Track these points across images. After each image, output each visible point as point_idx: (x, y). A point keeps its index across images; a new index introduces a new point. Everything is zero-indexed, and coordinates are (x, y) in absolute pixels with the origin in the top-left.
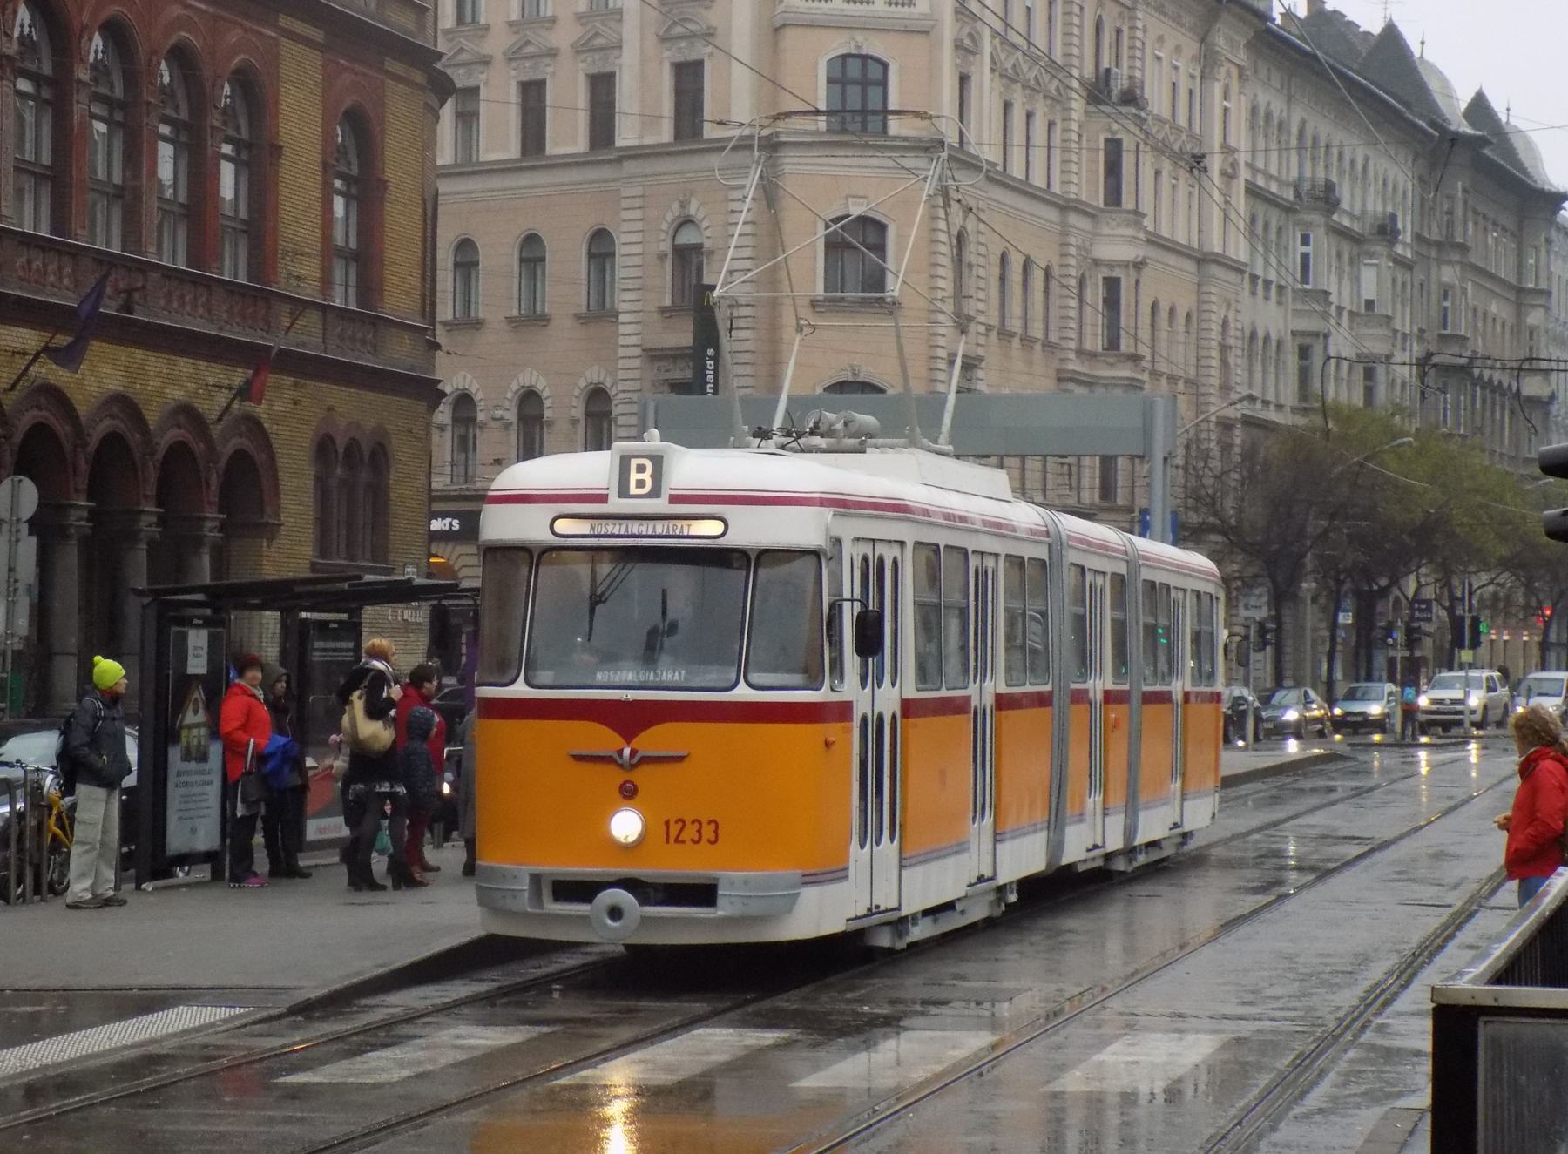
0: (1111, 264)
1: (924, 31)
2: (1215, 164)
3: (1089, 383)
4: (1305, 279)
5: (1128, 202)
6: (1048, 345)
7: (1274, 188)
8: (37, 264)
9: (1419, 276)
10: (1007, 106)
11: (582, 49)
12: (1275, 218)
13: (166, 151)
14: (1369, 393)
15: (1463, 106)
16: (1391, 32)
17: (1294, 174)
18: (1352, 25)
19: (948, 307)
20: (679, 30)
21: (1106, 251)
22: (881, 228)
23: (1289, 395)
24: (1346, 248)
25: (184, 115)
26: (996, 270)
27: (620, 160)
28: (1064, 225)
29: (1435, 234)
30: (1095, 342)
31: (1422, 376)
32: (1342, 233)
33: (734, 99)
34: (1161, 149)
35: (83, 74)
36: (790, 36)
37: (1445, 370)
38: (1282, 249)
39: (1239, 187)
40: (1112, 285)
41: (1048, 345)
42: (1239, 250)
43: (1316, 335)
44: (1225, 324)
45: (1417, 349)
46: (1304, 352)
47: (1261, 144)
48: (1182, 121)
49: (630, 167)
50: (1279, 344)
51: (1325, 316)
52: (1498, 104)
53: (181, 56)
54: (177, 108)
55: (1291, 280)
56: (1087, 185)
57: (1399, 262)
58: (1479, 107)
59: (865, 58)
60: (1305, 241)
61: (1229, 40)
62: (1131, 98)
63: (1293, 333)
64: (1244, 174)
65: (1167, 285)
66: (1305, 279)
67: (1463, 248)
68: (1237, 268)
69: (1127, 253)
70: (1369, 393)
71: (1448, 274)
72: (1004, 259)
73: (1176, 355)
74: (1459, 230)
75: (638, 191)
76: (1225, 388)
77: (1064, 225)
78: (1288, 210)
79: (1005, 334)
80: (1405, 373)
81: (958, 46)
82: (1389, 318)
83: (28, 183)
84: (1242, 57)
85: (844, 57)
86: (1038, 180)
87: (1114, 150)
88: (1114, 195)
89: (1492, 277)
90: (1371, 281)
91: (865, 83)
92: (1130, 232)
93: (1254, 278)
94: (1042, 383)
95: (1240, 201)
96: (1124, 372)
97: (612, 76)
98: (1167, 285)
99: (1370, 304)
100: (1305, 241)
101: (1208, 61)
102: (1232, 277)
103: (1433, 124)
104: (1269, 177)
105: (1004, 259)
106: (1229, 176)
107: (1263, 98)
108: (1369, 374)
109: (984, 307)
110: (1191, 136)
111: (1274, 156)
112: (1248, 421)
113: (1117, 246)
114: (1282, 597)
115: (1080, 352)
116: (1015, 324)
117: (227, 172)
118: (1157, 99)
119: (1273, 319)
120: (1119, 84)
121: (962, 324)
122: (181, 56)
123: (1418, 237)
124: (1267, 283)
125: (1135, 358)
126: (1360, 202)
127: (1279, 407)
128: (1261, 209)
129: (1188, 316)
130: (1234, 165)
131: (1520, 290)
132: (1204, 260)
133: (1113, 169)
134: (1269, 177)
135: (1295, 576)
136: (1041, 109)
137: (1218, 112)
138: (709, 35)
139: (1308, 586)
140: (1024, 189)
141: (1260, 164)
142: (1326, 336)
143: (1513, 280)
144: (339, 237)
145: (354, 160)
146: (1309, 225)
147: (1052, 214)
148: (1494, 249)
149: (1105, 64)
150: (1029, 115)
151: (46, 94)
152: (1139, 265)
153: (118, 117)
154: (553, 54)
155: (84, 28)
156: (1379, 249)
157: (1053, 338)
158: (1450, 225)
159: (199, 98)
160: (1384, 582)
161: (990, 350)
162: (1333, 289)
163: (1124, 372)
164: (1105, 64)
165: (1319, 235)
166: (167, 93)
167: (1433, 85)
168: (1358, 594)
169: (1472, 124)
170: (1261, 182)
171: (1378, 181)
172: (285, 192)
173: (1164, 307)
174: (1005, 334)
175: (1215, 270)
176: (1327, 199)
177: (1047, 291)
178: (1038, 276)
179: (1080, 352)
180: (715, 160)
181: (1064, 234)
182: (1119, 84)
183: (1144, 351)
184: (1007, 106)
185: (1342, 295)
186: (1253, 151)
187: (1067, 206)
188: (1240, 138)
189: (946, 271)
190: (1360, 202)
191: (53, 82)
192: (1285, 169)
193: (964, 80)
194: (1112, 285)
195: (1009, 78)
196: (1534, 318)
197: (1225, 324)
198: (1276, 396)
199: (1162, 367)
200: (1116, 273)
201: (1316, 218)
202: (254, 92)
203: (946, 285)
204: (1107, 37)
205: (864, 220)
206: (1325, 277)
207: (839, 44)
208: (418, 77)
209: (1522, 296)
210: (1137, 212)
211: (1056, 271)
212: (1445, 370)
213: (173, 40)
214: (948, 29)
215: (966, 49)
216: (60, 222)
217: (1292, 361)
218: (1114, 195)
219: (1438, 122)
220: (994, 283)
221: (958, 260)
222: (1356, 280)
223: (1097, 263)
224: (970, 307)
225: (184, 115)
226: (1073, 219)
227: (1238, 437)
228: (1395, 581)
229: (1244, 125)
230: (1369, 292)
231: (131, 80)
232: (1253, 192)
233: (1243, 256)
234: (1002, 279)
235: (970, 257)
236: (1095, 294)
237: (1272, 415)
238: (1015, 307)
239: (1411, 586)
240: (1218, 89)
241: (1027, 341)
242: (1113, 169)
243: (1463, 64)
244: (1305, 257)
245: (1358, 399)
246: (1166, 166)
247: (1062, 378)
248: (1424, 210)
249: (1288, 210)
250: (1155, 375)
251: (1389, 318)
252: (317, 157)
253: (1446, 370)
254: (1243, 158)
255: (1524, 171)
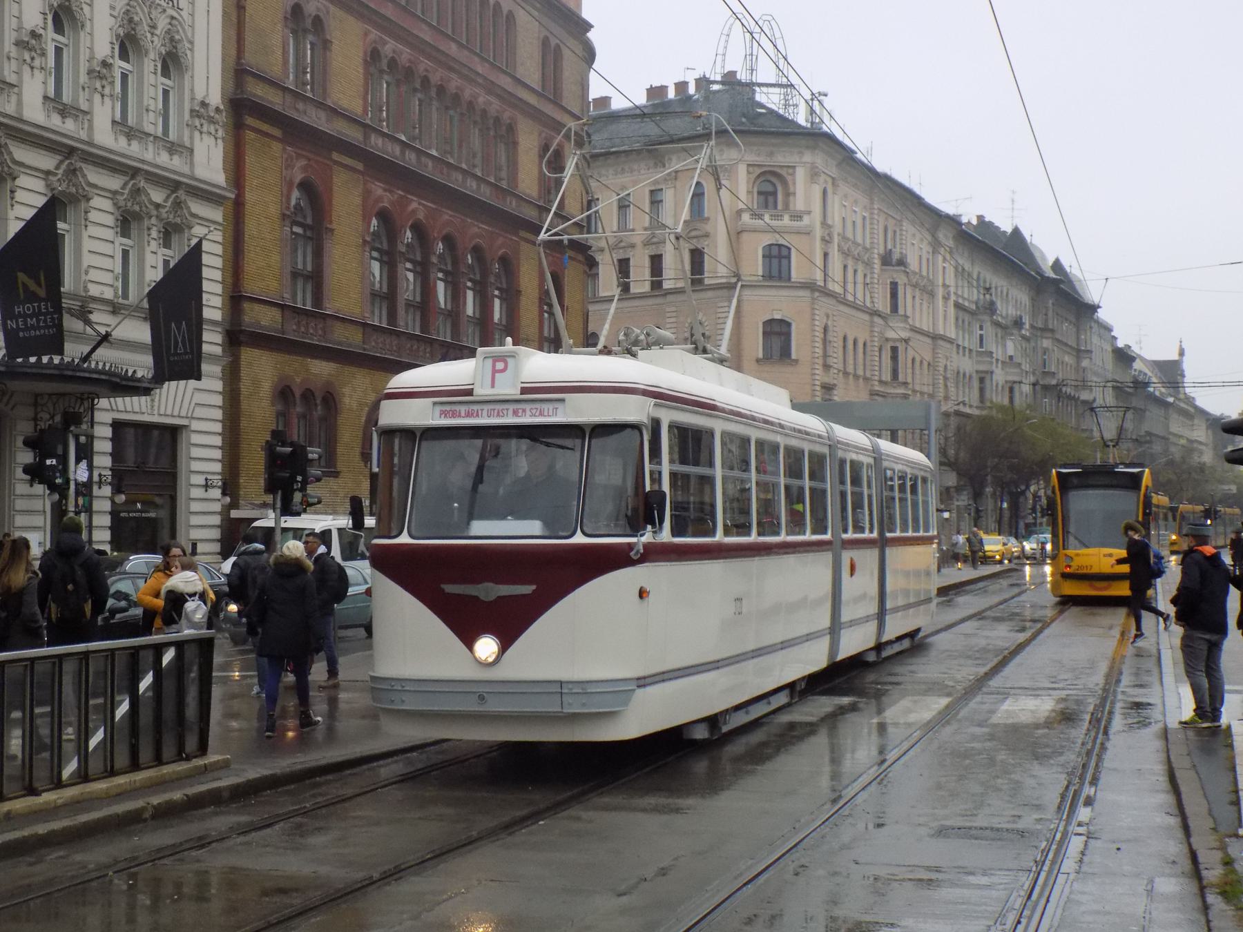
0: (894, 340)
1: (808, 233)
2: (940, 292)
3: (884, 396)
4: (981, 346)
5: (901, 311)
6: (866, 379)
7: (966, 304)
8: (388, 341)
9: (1033, 344)
10: (845, 267)
11: (647, 243)
12: (967, 317)
13: (470, 295)
14: (1011, 399)
15: (1050, 264)
16: (1016, 232)
17: (975, 297)
18: (997, 228)
19: (820, 361)
20: (693, 233)
21: (891, 334)
22: (789, 325)
23: (975, 402)
24: (999, 331)
25: (478, 277)
26: (841, 343)
27: (665, 295)
28: (872, 322)
29: (1040, 325)
30: (887, 377)
31: (1034, 390)
32: (997, 324)
33: (718, 267)
34: (915, 286)
35: (434, 260)
36: (745, 236)
37: (1048, 389)
38: (971, 333)
39: (951, 303)
40: (894, 350)
41: (866, 379)
42: (952, 334)
43: (986, 372)
44: (946, 366)
45: (1032, 379)
46: (982, 380)
47: (960, 283)
48: (924, 273)
49: (670, 298)
50: (971, 377)
51: (991, 363)
52: (1066, 263)
53: (477, 251)
54: (305, 217)
55: (975, 344)
56: (882, 303)
57: (1024, 337)
58: (1057, 265)
59: (780, 246)
60: (981, 328)
61: (946, 236)
62: (902, 262)
63: (977, 372)
64: (953, 298)
65: (921, 349)
66: (981, 346)
67: (1052, 331)
68: (950, 341)
69: (904, 335)
70: (1011, 399)
71: (1046, 343)
72: (845, 339)
73: (921, 381)
74: (1050, 322)
75: (674, 309)
76: (946, 398)
77: (872, 322)
78: (972, 313)
79: (846, 374)
80: (1026, 388)
81: (823, 239)
82: (1020, 364)
83: (378, 300)
84: (951, 243)
85: (770, 245)
86: (850, 298)
87: (894, 286)
88: (895, 308)
89: (1066, 345)
90: (1011, 348)
91: (780, 257)
92: (902, 325)
93: (958, 346)
94: (863, 396)
95: (952, 311)
96: (901, 391)
97: (660, 256)
98: (921, 349)
99: (1011, 357)
100: (981, 328)
101: (936, 245)
102: (948, 346)
103: (1038, 273)
104: (964, 299)
105: (845, 339)
106: (946, 298)
107: (961, 262)
108: (1011, 390)
109: (836, 361)
110: (929, 280)
111: (966, 289)
112: (958, 413)
113: (896, 331)
114: (977, 495)
115: (881, 382)
116: (850, 369)
117: (441, 287)
118: (913, 263)
119: (967, 365)
120: (896, 256)
121: (827, 367)
122: (477, 251)
123: (1032, 326)
124: (970, 350)
125: (905, 384)
126: (1007, 310)
127: (971, 406)
128: (961, 314)
129: (865, 344)
130: (949, 294)
131: (1079, 351)
132: (935, 337)
133: (894, 295)
134: (964, 299)
135: (982, 485)
136: (860, 268)
137: (940, 269)
138: (707, 235)
139: (989, 490)
140: (845, 303)
141: (960, 293)
142: (992, 373)
143: (1074, 345)
144: (546, 334)
145: (504, 281)
146: (982, 321)
147: (867, 317)
148: (1066, 330)
149: (889, 247)
150: (855, 271)
151: (419, 269)
152: (906, 341)
153: (385, 258)
154: (633, 246)
155: (435, 239)
156: (1015, 332)
157: (868, 374)
158: (1046, 320)
159: (485, 272)
160: (1023, 487)
161: (840, 381)
162: (994, 350)
163: (901, 391)
164: (889, 247)
165: (988, 325)
166: (471, 267)
167: (1037, 255)
168: (1011, 493)
169: (1055, 273)
170: (960, 301)
171: (1014, 300)
172: (522, 312)
173: (918, 359)
174: (846, 374)
175: (941, 342)
176: (991, 308)
177: (864, 353)
178: (860, 345)
179: (881, 382)
180: (710, 294)
181: (872, 326)
182: (896, 256)
183: (909, 380)
184: (845, 267)
185: (998, 353)
186: (957, 287)
187: (875, 313)
188: (951, 280)
189: (819, 344)
190: (1007, 310)
191: (387, 253)
192: (971, 296)
193: (826, 255)
194: (894, 350)
195: (845, 254)
196: (1085, 363)
197: (946, 366)
198: (968, 400)
199: (917, 388)
200: (898, 344)
201: (986, 318)
202: (508, 265)
203: (819, 351)
204: (890, 235)
205: (781, 321)
206: (991, 345)
207: (768, 239)
208: (580, 257)
209: (1079, 353)
210: (906, 317)
211: (869, 344)
212: (1048, 389)
213: (473, 243)
214: (818, 232)
215: (826, 241)
216: (425, 327)
217: (976, 384)
218: (895, 308)
219: (1040, 272)
220: (841, 349)
221: (825, 341)
222: (1005, 346)
223: (887, 340)
224: (830, 361)
225: (478, 277)
226: (876, 319)
227: (953, 421)
228: (1028, 487)
229: (952, 275)
230: (1010, 351)
231: (455, 262)
232: (957, 306)
233: (953, 336)
234: (844, 347)
235: (830, 338)
236: (887, 355)
237: (967, 410)
238: (850, 361)
239: (1032, 488)
240: (940, 258)
241: (856, 377)
242: (894, 295)
243: (1049, 246)
244: (981, 336)
245: (1006, 401)
246: (918, 293)
247: (873, 394)
248: (1034, 315)
249: (972, 313)
250: (914, 391)
251: (1020, 364)
252: (537, 295)
253: (1046, 388)
254: (952, 290)
255: (1077, 292)
